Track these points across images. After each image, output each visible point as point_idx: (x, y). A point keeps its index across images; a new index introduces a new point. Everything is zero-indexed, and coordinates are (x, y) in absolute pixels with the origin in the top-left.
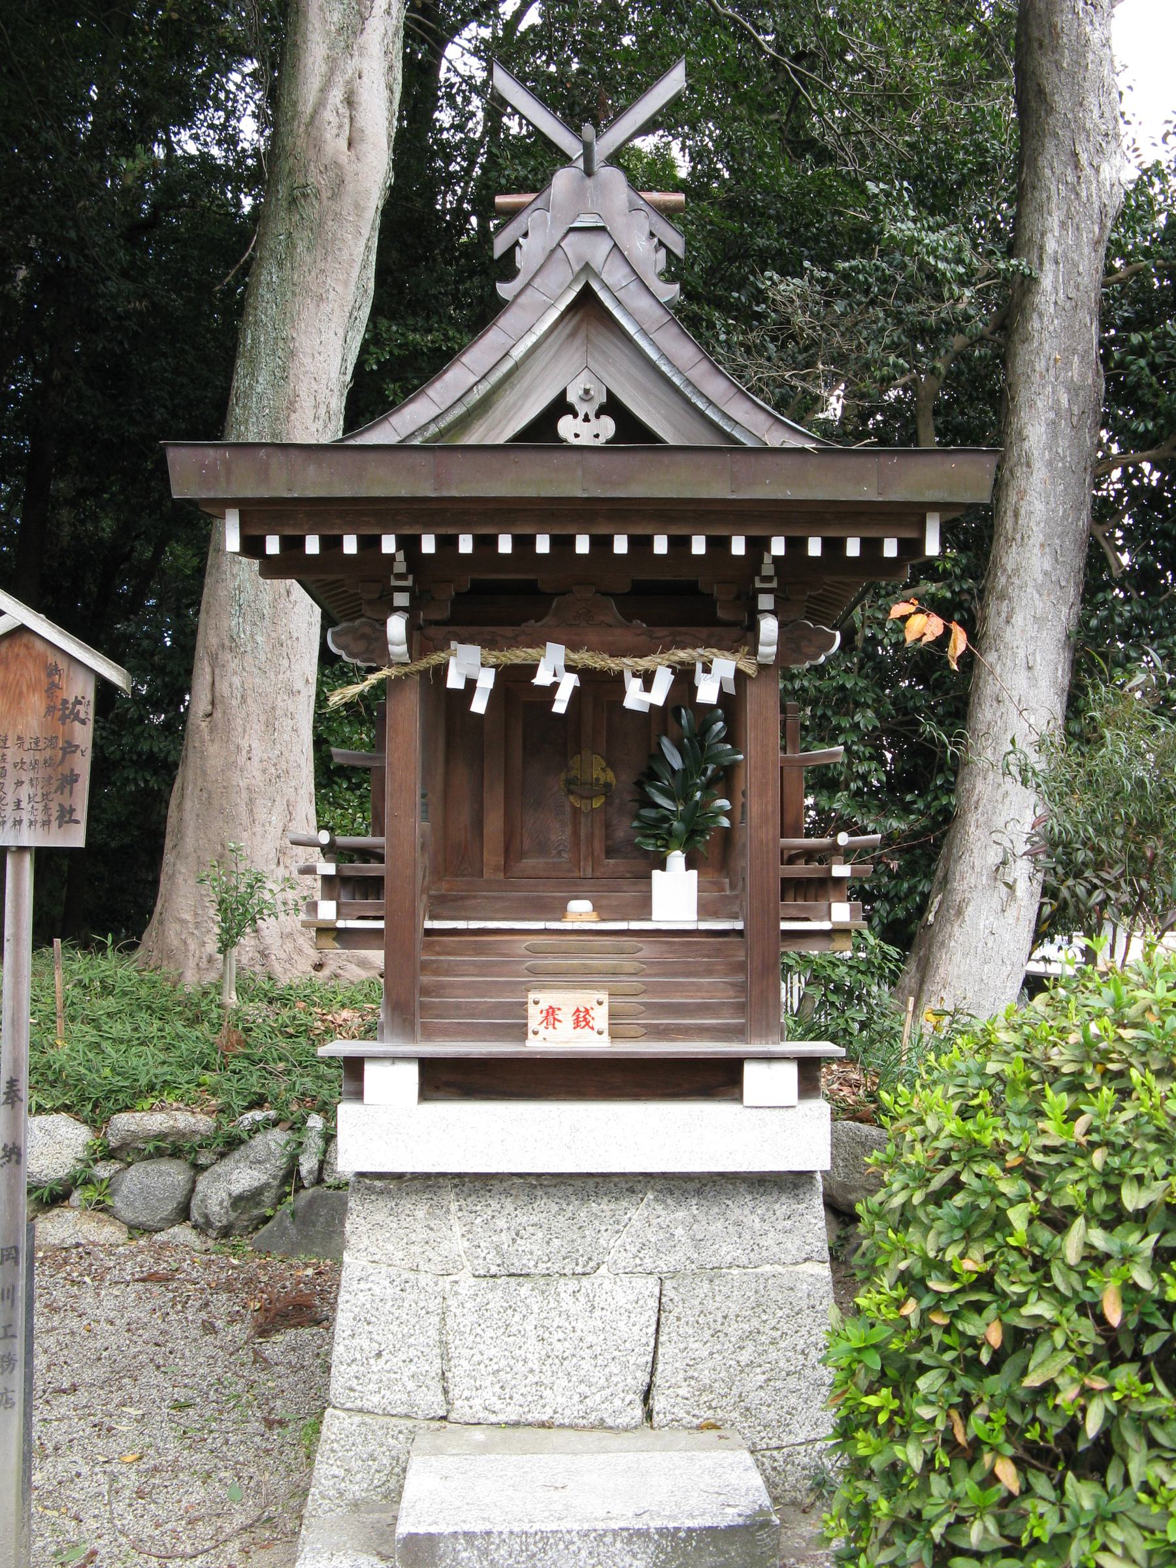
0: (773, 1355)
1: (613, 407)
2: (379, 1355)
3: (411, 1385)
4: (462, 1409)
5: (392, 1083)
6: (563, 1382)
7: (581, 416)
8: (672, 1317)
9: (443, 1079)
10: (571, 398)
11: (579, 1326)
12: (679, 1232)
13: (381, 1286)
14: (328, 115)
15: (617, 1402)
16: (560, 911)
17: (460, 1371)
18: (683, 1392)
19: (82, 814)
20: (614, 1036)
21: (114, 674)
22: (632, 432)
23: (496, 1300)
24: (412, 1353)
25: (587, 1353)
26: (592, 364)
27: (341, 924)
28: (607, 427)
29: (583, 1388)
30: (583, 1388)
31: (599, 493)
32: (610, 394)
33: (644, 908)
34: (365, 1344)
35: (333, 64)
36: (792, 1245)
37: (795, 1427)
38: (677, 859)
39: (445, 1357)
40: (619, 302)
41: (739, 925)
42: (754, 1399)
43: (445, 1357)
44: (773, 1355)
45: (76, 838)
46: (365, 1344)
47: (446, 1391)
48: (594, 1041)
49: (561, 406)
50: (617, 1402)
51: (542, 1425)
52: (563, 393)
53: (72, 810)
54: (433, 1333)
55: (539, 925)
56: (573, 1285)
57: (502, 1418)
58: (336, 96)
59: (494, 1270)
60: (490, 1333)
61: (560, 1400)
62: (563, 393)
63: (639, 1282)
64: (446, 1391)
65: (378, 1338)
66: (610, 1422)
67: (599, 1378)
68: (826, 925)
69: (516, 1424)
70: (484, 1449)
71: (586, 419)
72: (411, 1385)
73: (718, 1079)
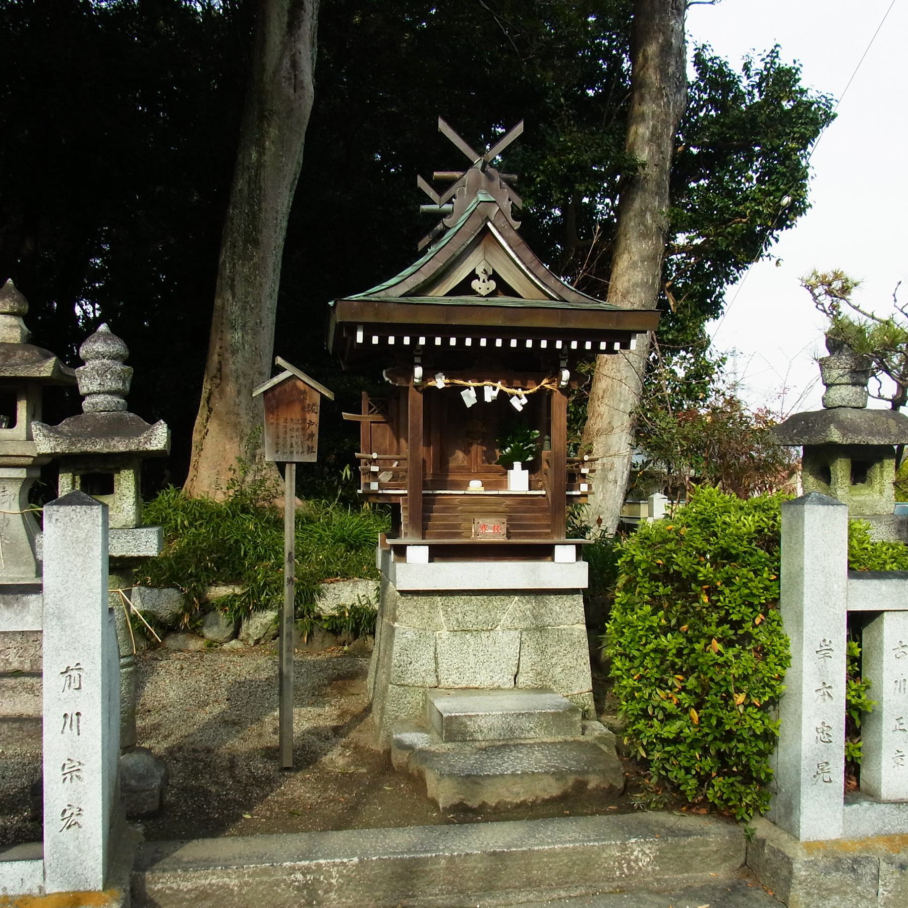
0: (565, 660)
1: (495, 276)
2: (411, 663)
3: (423, 674)
4: (444, 683)
5: (418, 554)
6: (484, 672)
7: (481, 280)
8: (526, 645)
9: (438, 553)
10: (477, 272)
11: (490, 650)
12: (528, 613)
13: (410, 635)
14: (284, 73)
15: (505, 679)
16: (466, 485)
17: (443, 667)
18: (531, 675)
19: (316, 449)
20: (508, 537)
21: (328, 394)
22: (503, 288)
23: (457, 640)
24: (424, 661)
25: (493, 660)
26: (487, 258)
27: (380, 492)
28: (493, 285)
29: (491, 674)
30: (491, 674)
31: (508, 324)
32: (494, 270)
33: (503, 484)
34: (405, 658)
35: (285, 45)
36: (571, 618)
37: (573, 688)
38: (517, 465)
39: (437, 663)
40: (500, 233)
41: (406, 492)
42: (558, 677)
43: (437, 663)
44: (565, 660)
45: (313, 458)
46: (405, 658)
47: (437, 677)
48: (501, 539)
49: (473, 276)
50: (505, 679)
51: (477, 688)
52: (474, 270)
53: (313, 447)
54: (432, 654)
55: (496, 493)
56: (487, 634)
57: (460, 686)
58: (286, 63)
59: (456, 628)
60: (454, 653)
61: (482, 680)
62: (474, 270)
63: (513, 633)
64: (437, 677)
65: (411, 656)
66: (502, 687)
67: (497, 669)
68: (578, 493)
69: (466, 688)
70: (454, 696)
71: (484, 281)
72: (423, 674)
73: (545, 552)
